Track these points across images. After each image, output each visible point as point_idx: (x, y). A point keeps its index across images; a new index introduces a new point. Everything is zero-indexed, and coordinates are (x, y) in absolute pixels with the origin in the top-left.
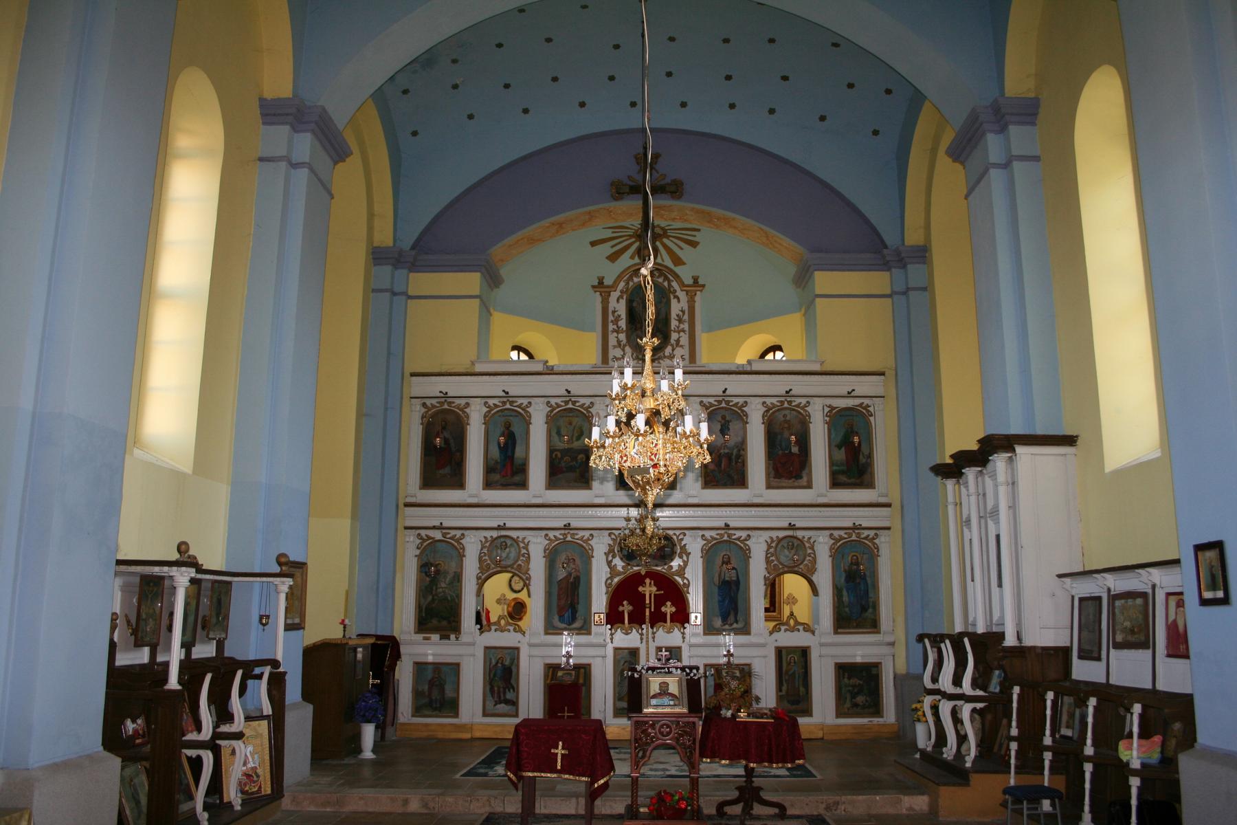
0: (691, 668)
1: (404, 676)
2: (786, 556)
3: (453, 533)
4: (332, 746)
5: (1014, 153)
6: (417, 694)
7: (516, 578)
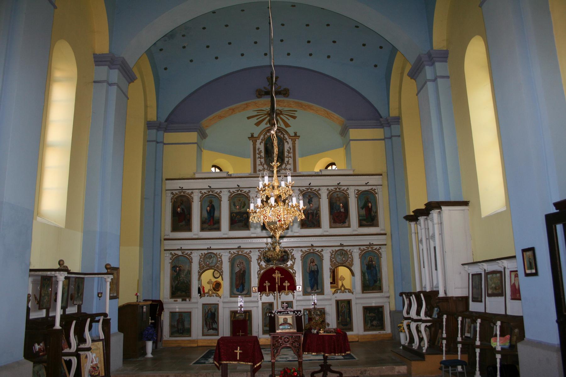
0: (298, 311)
1: (166, 318)
3: (187, 252)
6: (172, 326)
7: (216, 272)
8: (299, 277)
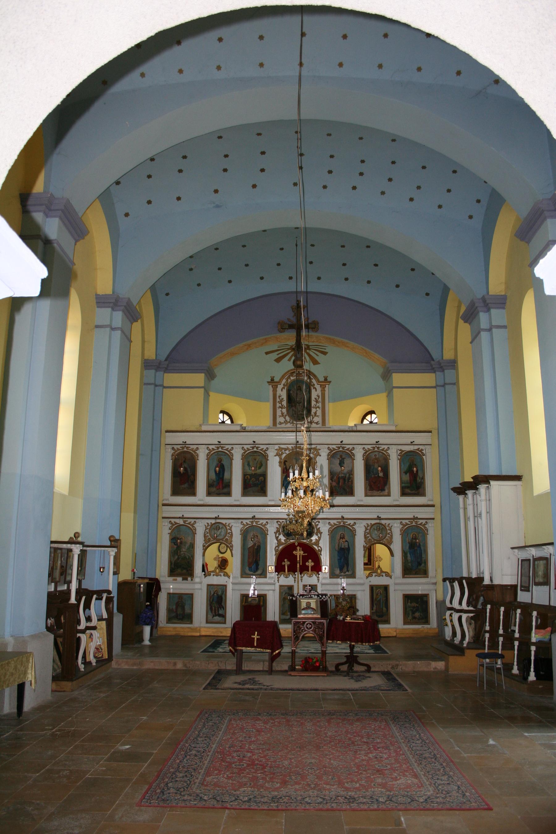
0: (322, 595)
1: (162, 601)
2: (375, 534)
3: (189, 520)
4: (131, 639)
5: (493, 324)
6: (169, 610)
7: (223, 545)
8: (326, 556)
